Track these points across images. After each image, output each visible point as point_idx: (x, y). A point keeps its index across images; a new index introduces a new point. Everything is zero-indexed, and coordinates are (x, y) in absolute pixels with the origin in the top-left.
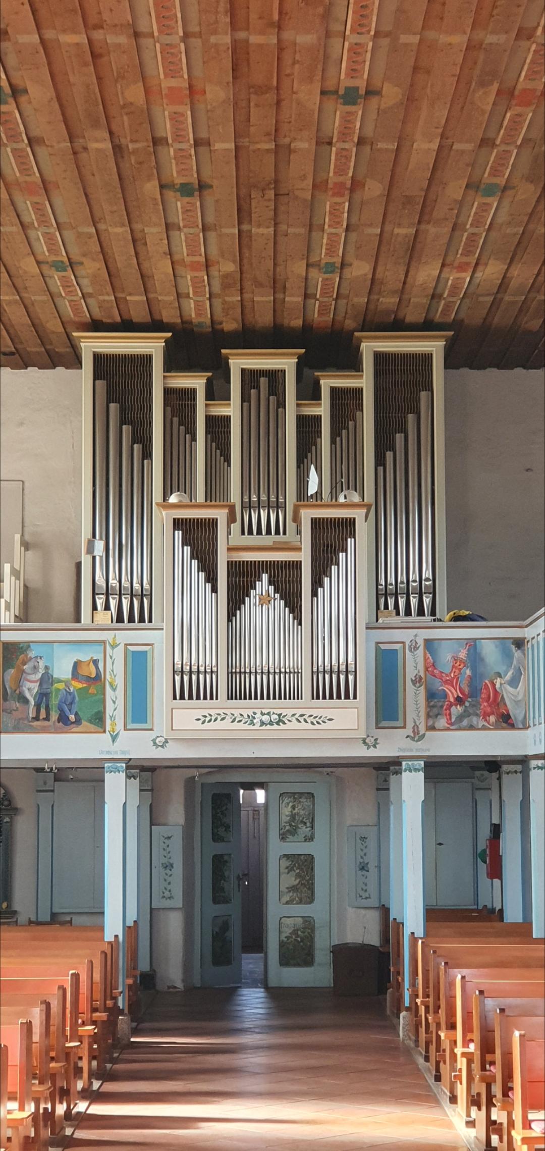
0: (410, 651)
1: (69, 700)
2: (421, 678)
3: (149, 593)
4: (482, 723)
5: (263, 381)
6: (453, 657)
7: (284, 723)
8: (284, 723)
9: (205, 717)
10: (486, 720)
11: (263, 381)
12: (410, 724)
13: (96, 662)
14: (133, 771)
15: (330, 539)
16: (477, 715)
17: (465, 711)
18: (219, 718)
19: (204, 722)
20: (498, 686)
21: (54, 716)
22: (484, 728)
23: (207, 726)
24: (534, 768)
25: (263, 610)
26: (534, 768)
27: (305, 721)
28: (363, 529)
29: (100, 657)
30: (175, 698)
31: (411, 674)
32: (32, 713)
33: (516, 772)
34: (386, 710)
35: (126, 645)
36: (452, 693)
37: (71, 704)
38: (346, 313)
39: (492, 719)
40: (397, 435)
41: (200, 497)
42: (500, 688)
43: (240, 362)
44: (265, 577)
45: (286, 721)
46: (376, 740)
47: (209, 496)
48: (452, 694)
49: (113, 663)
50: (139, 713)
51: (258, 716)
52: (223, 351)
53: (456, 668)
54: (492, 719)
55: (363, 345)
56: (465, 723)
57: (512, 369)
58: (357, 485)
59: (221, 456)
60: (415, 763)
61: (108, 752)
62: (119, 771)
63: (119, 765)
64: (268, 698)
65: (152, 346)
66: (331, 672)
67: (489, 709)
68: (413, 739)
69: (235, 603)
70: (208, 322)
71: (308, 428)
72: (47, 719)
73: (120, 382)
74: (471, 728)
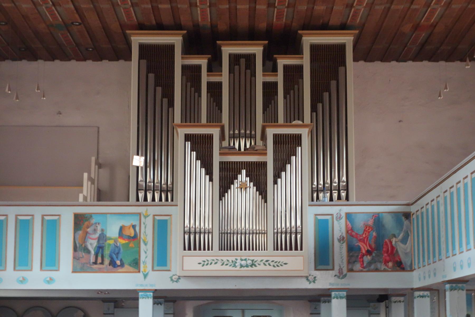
0: (337, 220)
1: (116, 251)
2: (343, 238)
3: (171, 189)
4: (383, 267)
5: (243, 61)
6: (364, 224)
7: (255, 266)
8: (255, 266)
9: (204, 261)
10: (386, 265)
11: (243, 61)
12: (337, 268)
13: (134, 227)
14: (159, 300)
15: (286, 147)
16: (380, 262)
17: (372, 259)
18: (214, 262)
19: (203, 265)
20: (393, 243)
21: (107, 261)
22: (385, 271)
23: (205, 268)
24: (418, 297)
25: (242, 196)
26: (418, 297)
27: (269, 265)
28: (306, 141)
29: (136, 223)
30: (185, 249)
31: (337, 235)
32: (92, 259)
33: (400, 301)
34: (323, 258)
35: (154, 215)
36: (364, 248)
37: (118, 253)
38: (293, 17)
39: (390, 264)
40: (324, 93)
41: (204, 120)
42: (395, 244)
43: (228, 50)
44: (244, 172)
45: (257, 265)
46: (315, 277)
47: (209, 119)
48: (364, 248)
49: (145, 227)
50: (161, 260)
51: (239, 261)
52: (218, 42)
53: (366, 231)
54: (390, 264)
55: (304, 38)
56: (373, 267)
57: (390, 62)
58: (300, 117)
59: (216, 106)
60: (341, 293)
61: (141, 285)
62: (148, 298)
63: (148, 293)
64: (245, 249)
65: (175, 40)
66: (286, 233)
67: (388, 258)
68: (339, 277)
69: (224, 188)
70: (209, 24)
71: (270, 89)
72: (102, 263)
73: (157, 62)
74: (377, 270)
